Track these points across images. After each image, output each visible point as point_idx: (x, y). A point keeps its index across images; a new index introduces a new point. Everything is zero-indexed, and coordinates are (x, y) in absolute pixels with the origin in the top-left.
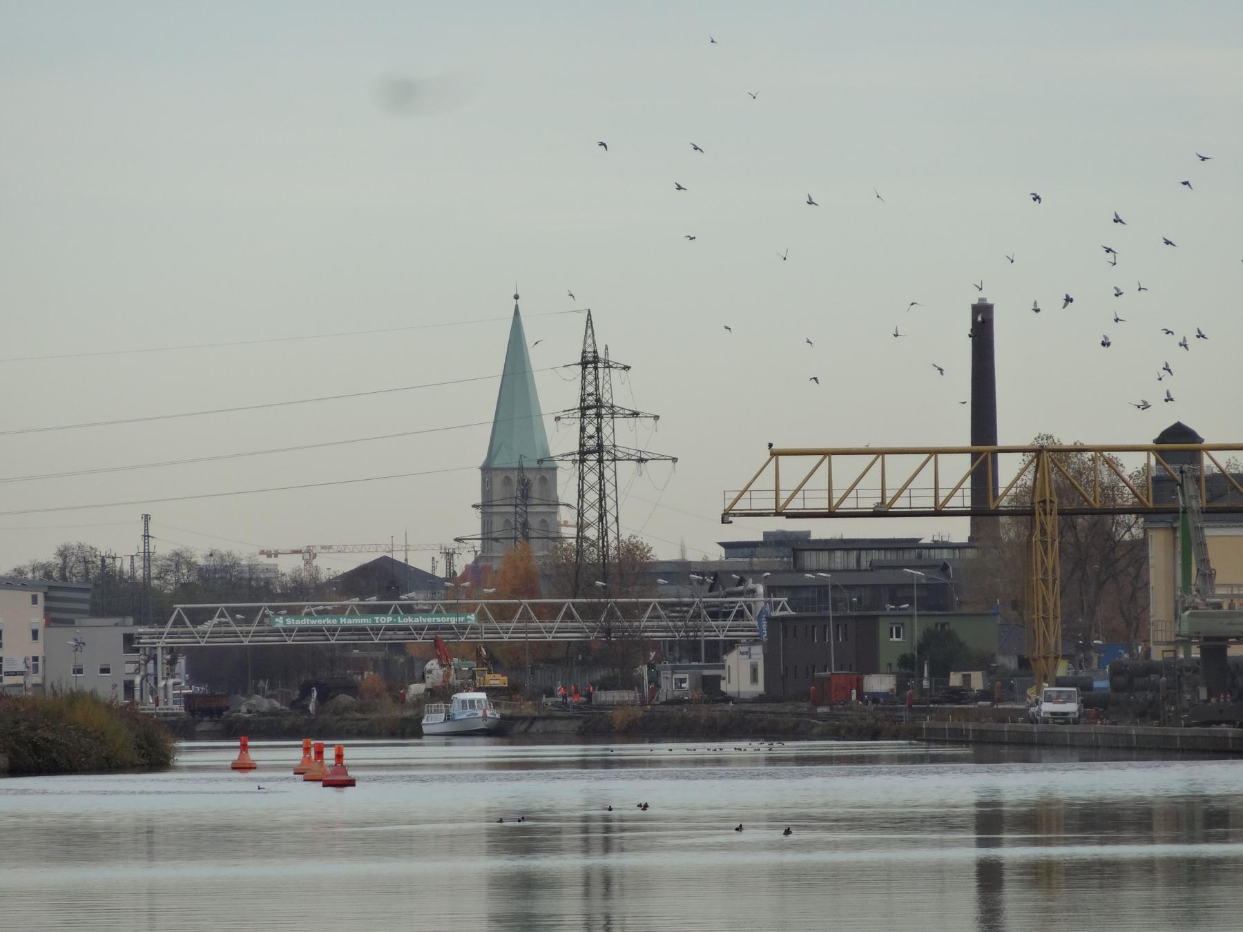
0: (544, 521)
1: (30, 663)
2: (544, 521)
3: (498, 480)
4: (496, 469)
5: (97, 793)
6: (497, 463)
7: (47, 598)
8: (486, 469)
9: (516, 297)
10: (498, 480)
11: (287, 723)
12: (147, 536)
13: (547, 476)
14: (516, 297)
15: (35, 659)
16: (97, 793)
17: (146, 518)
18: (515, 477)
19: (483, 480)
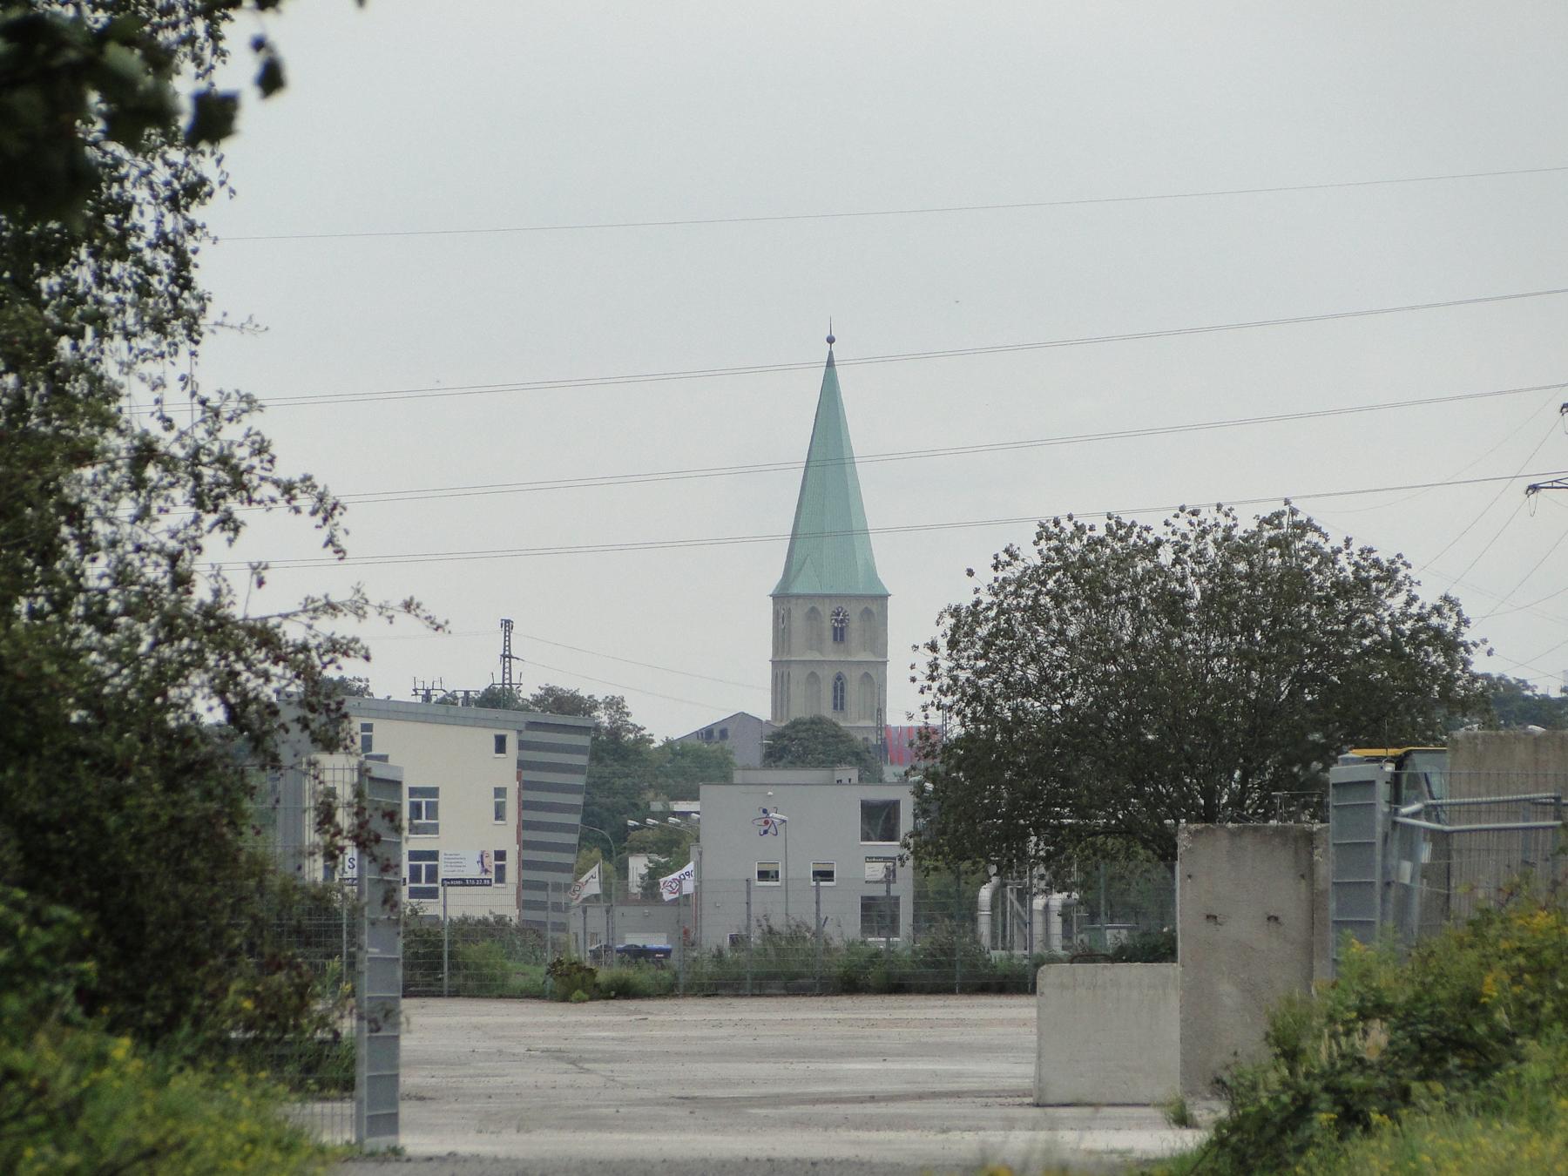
0: (867, 675)
1: (491, 863)
2: (867, 675)
3: (798, 613)
4: (798, 596)
5: (1001, 1022)
6: (797, 589)
7: (523, 745)
8: (781, 598)
9: (831, 340)
10: (798, 613)
11: (603, 976)
12: (507, 656)
13: (874, 608)
14: (831, 340)
15: (500, 855)
16: (1001, 1022)
17: (507, 625)
18: (826, 610)
19: (776, 613)
